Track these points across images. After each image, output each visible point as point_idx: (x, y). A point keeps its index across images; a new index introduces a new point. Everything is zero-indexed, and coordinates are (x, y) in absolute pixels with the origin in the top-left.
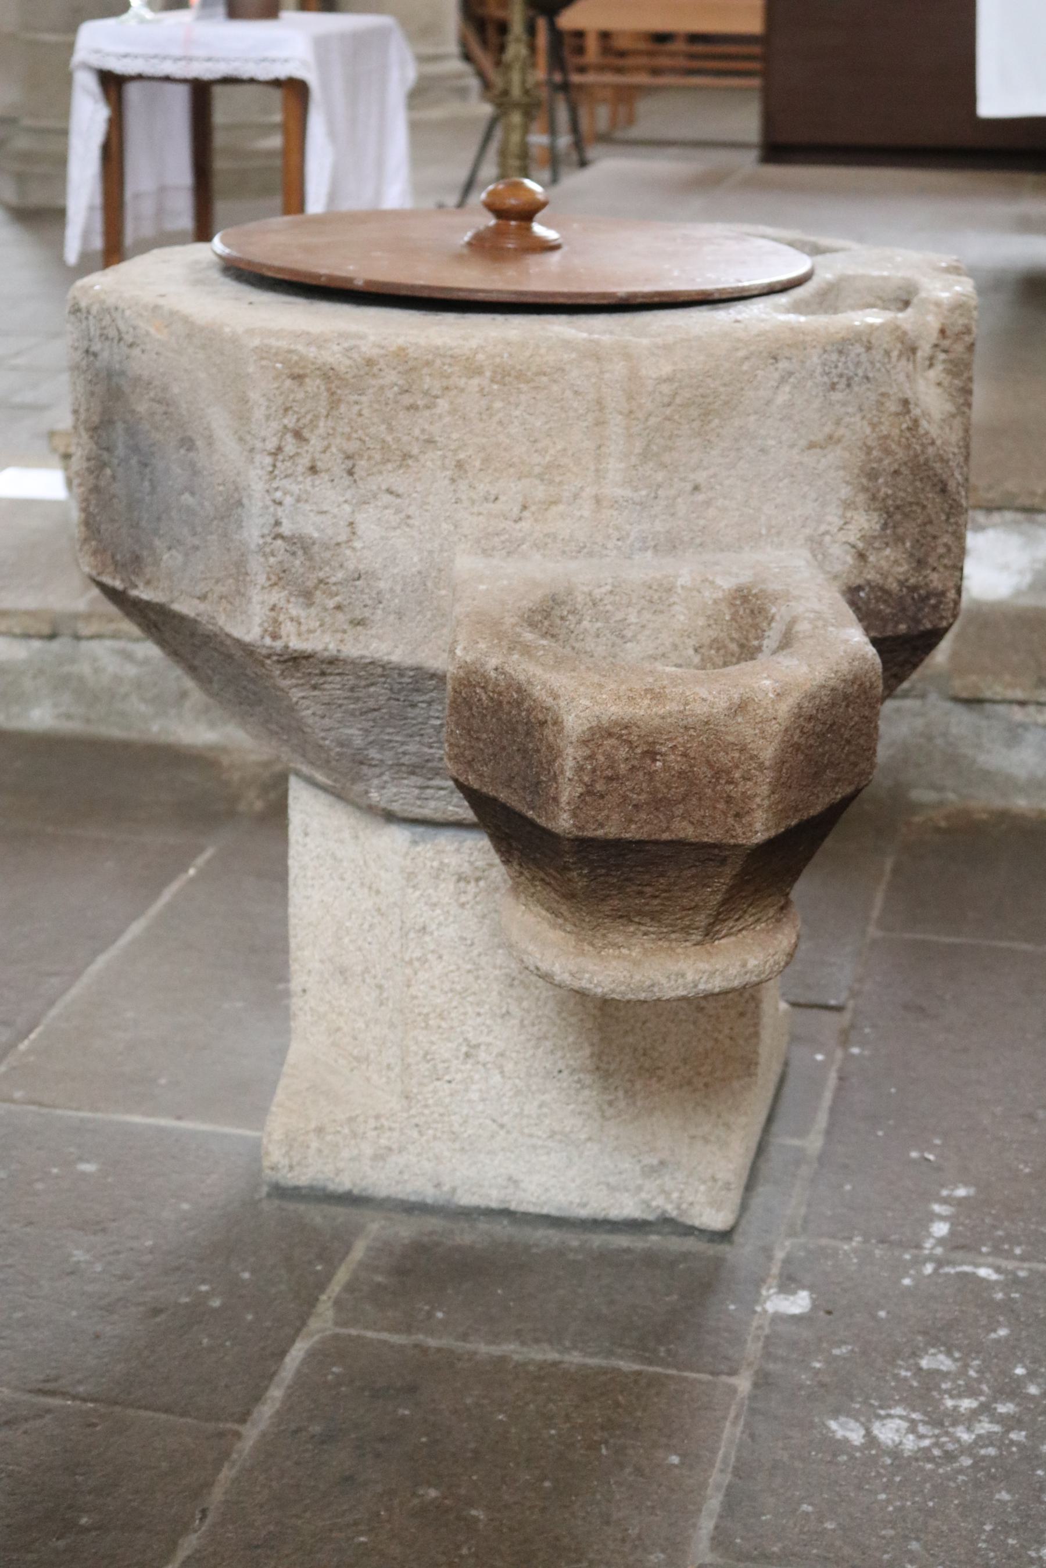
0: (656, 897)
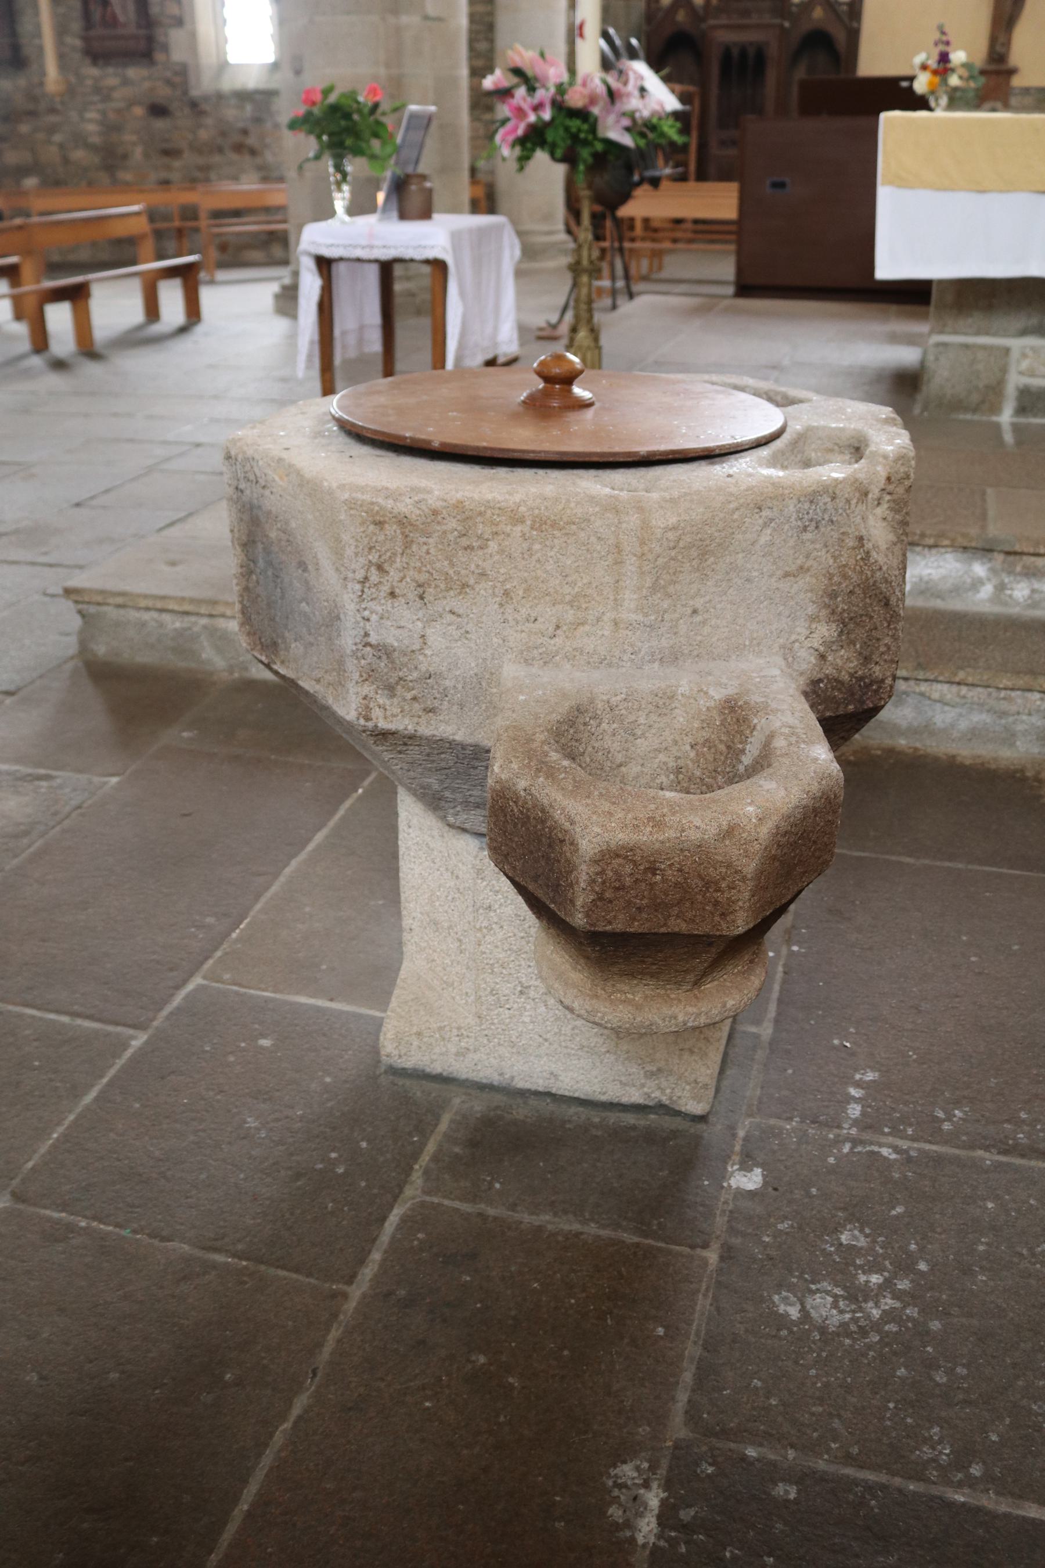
0: (655, 964)
